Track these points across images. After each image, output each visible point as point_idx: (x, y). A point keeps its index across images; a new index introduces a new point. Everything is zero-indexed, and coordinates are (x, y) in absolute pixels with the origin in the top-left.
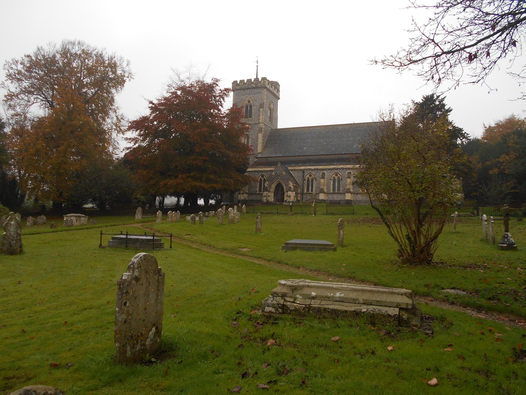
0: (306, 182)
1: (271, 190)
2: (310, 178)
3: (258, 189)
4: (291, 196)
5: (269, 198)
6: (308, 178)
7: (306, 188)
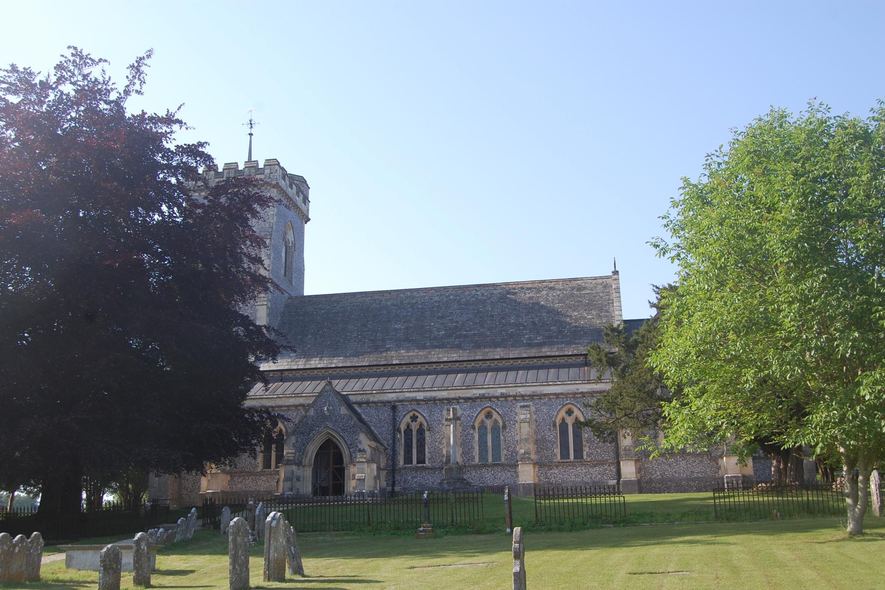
0: (401, 437)
1: (306, 461)
2: (414, 427)
3: (557, 451)
4: (362, 475)
5: (298, 485)
6: (408, 426)
7: (402, 452)
